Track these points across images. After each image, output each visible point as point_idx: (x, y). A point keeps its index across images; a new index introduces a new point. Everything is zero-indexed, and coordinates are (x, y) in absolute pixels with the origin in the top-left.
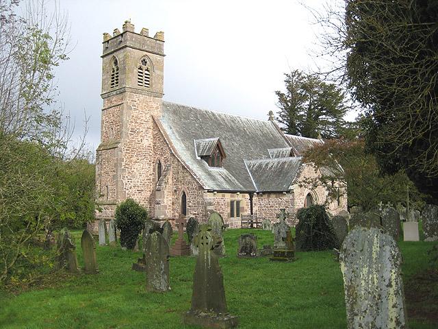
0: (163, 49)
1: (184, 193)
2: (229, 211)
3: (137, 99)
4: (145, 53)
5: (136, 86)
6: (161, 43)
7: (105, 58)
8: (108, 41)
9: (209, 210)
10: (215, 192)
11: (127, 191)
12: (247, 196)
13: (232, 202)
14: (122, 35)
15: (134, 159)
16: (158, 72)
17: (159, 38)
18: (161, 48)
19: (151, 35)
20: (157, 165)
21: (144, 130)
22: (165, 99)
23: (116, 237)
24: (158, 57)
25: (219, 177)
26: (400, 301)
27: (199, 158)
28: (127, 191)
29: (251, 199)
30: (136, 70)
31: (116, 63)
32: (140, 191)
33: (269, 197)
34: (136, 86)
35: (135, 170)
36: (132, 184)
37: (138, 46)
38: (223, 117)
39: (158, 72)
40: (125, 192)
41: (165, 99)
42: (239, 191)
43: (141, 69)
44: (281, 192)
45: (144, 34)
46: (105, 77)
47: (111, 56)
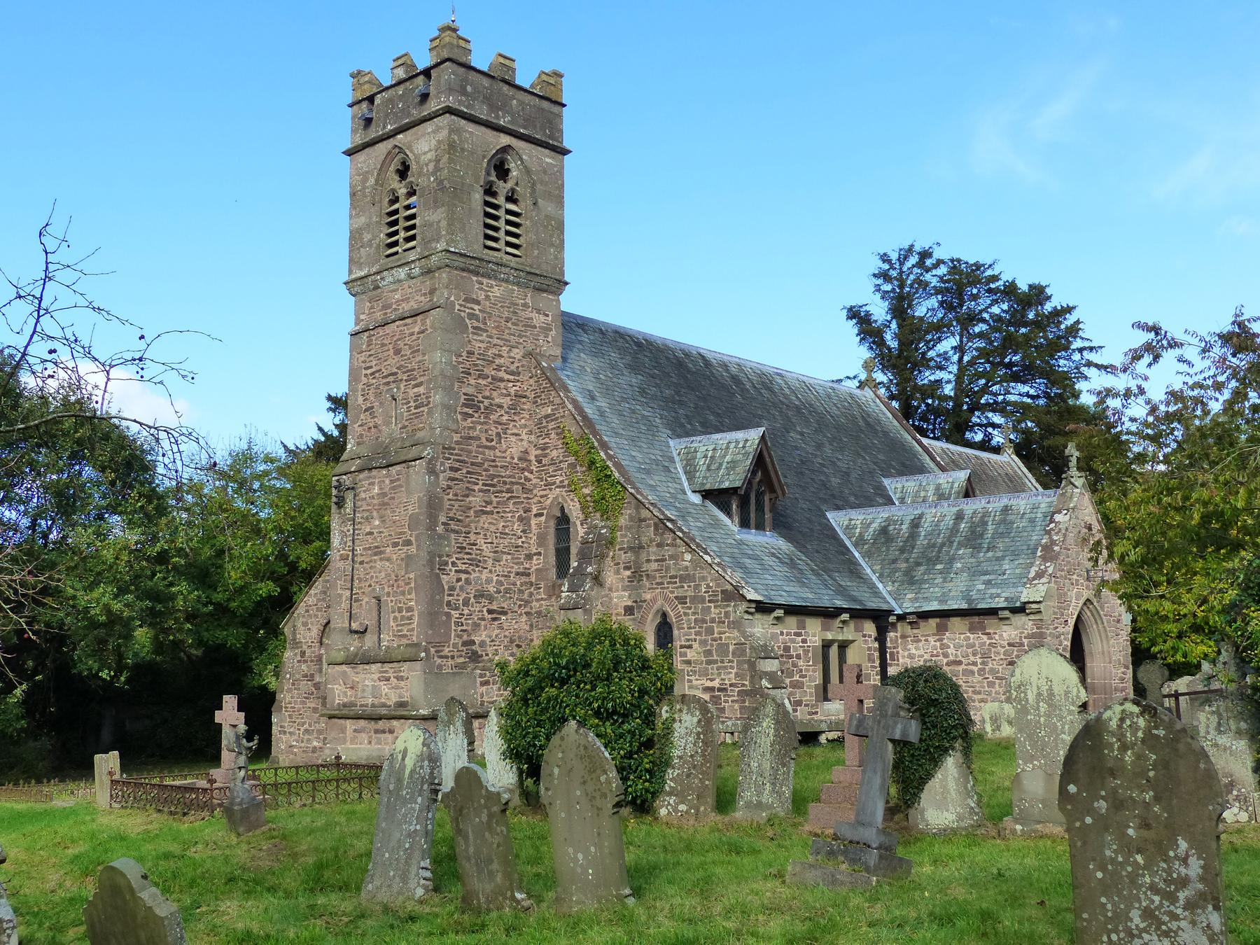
0: (561, 131)
1: (664, 615)
2: (819, 680)
3: (482, 296)
4: (505, 140)
5: (477, 249)
6: (556, 109)
7: (361, 157)
8: (371, 99)
9: (766, 673)
10: (845, 616)
11: (455, 614)
12: (870, 628)
13: (826, 645)
14: (427, 73)
15: (476, 500)
16: (547, 207)
17: (548, 97)
18: (554, 124)
19: (524, 78)
20: (552, 523)
21: (506, 401)
22: (570, 302)
23: (1039, 822)
24: (548, 158)
25: (770, 561)
26: (51, 788)
27: (696, 499)
28: (455, 614)
29: (881, 639)
30: (478, 196)
31: (403, 172)
32: (496, 614)
33: (941, 629)
34: (477, 249)
35: (480, 541)
36: (472, 590)
37: (482, 112)
38: (734, 370)
39: (547, 207)
40: (448, 615)
41: (570, 302)
42: (780, 606)
43: (515, 201)
44: (993, 612)
45: (502, 76)
46: (362, 220)
47: (383, 148)
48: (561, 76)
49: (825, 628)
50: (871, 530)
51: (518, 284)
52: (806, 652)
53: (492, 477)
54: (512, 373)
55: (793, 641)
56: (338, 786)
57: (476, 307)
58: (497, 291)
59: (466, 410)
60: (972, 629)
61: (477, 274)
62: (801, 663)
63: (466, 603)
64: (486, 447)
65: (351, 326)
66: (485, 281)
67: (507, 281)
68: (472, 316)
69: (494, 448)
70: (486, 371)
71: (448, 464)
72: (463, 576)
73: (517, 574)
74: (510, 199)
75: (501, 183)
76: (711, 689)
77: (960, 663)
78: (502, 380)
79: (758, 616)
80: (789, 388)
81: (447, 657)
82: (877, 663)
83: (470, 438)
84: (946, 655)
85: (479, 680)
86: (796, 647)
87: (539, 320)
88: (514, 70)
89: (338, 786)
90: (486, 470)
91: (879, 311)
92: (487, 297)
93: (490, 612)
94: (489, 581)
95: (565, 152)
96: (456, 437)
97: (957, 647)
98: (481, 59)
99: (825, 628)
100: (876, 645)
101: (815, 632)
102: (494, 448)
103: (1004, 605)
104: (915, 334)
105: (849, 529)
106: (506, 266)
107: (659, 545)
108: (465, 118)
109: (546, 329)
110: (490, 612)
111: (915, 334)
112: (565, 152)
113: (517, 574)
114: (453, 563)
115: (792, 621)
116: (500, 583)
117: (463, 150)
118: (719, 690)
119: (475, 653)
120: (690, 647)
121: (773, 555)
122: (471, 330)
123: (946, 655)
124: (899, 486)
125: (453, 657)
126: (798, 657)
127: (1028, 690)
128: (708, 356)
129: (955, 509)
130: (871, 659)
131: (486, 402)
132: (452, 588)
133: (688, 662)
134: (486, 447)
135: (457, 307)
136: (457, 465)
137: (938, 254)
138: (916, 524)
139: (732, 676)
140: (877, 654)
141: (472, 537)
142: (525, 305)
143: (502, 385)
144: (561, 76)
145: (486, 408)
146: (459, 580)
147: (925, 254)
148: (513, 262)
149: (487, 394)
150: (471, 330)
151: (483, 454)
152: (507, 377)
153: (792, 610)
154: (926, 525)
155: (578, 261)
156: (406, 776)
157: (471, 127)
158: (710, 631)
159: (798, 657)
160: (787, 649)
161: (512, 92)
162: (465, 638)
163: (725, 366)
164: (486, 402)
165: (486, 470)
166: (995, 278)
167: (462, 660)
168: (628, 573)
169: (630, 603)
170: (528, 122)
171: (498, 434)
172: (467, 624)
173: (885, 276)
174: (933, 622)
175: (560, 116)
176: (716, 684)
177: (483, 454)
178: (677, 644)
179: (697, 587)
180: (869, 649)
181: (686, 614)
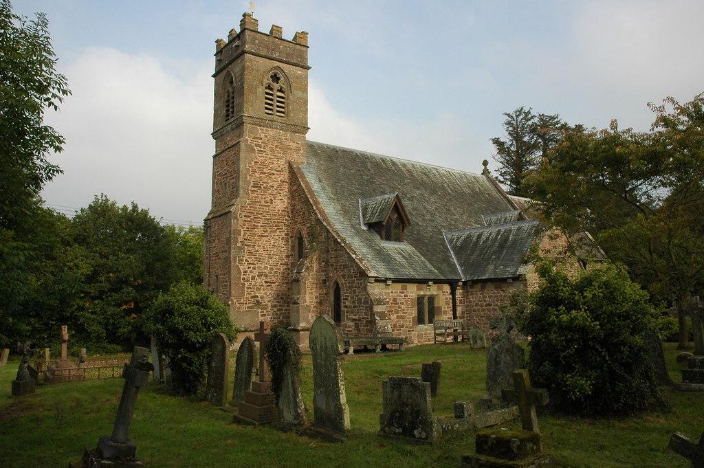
1: (337, 284)
4: (277, 64)
12: (447, 288)
15: (259, 231)
17: (300, 41)
20: (297, 241)
21: (276, 185)
22: (311, 136)
24: (299, 71)
27: (365, 228)
33: (483, 288)
36: (256, 272)
38: (409, 167)
40: (244, 284)
41: (311, 136)
44: (504, 280)
48: (307, 34)
49: (419, 289)
50: (460, 240)
51: (282, 129)
52: (407, 301)
53: (268, 220)
54: (279, 171)
55: (399, 296)
56: (113, 370)
57: (259, 141)
58: (271, 133)
59: (253, 189)
60: (496, 288)
61: (260, 126)
62: (403, 307)
63: (253, 278)
64: (265, 206)
65: (214, 153)
66: (264, 129)
67: (276, 128)
68: (257, 145)
69: (269, 206)
70: (265, 170)
71: (243, 214)
72: (252, 266)
73: (281, 264)
74: (280, 91)
75: (275, 84)
76: (355, 320)
77: (491, 305)
78: (273, 174)
79: (376, 284)
80: (439, 174)
81: (242, 303)
82: (451, 305)
83: (256, 202)
84: (485, 301)
85: (260, 314)
86: (401, 298)
87: (293, 145)
88: (281, 32)
89: (113, 370)
90: (264, 216)
91: (506, 138)
92: (266, 136)
93: (266, 282)
94: (266, 268)
95: (308, 68)
96: (248, 201)
97: (490, 297)
98: (264, 28)
99: (419, 289)
100: (451, 296)
101: (413, 291)
102: (269, 206)
103: (510, 276)
104: (525, 148)
105: (451, 241)
106: (275, 121)
107: (335, 250)
108: (253, 55)
109: (298, 150)
110: (266, 282)
111: (525, 148)
112: (308, 68)
113: (281, 264)
114: (246, 260)
115: (399, 286)
116: (272, 269)
117: (253, 69)
118: (359, 320)
119: (258, 301)
120: (347, 299)
121: (400, 253)
122: (257, 152)
123: (485, 301)
124: (489, 219)
125: (246, 304)
126: (402, 303)
127: (29, 343)
128: (396, 161)
129: (497, 229)
130: (447, 303)
131: (265, 185)
132: (245, 272)
133: (346, 307)
134: (265, 206)
135: (249, 141)
136: (249, 214)
137: (533, 113)
138: (479, 236)
139: (363, 314)
140: (451, 301)
141: (257, 248)
142: (286, 139)
143: (273, 177)
144: (307, 34)
145: (264, 188)
146: (249, 268)
147: (527, 114)
148: (280, 120)
149: (265, 181)
150: (257, 152)
151: (263, 209)
152: (276, 173)
153: (395, 281)
154: (484, 238)
155: (313, 119)
156: (231, 362)
157: (258, 59)
158: (355, 292)
159: (402, 303)
160: (395, 300)
161: (280, 42)
162: (253, 294)
163: (404, 165)
164: (265, 185)
165: (264, 216)
166: (558, 123)
167: (251, 305)
168: (324, 264)
169: (324, 278)
170: (288, 55)
171: (271, 200)
172: (254, 288)
173: (509, 123)
174: (479, 285)
175: (306, 52)
176: (357, 317)
177: (263, 209)
178: (342, 298)
179: (350, 271)
180: (446, 299)
181: (345, 283)
